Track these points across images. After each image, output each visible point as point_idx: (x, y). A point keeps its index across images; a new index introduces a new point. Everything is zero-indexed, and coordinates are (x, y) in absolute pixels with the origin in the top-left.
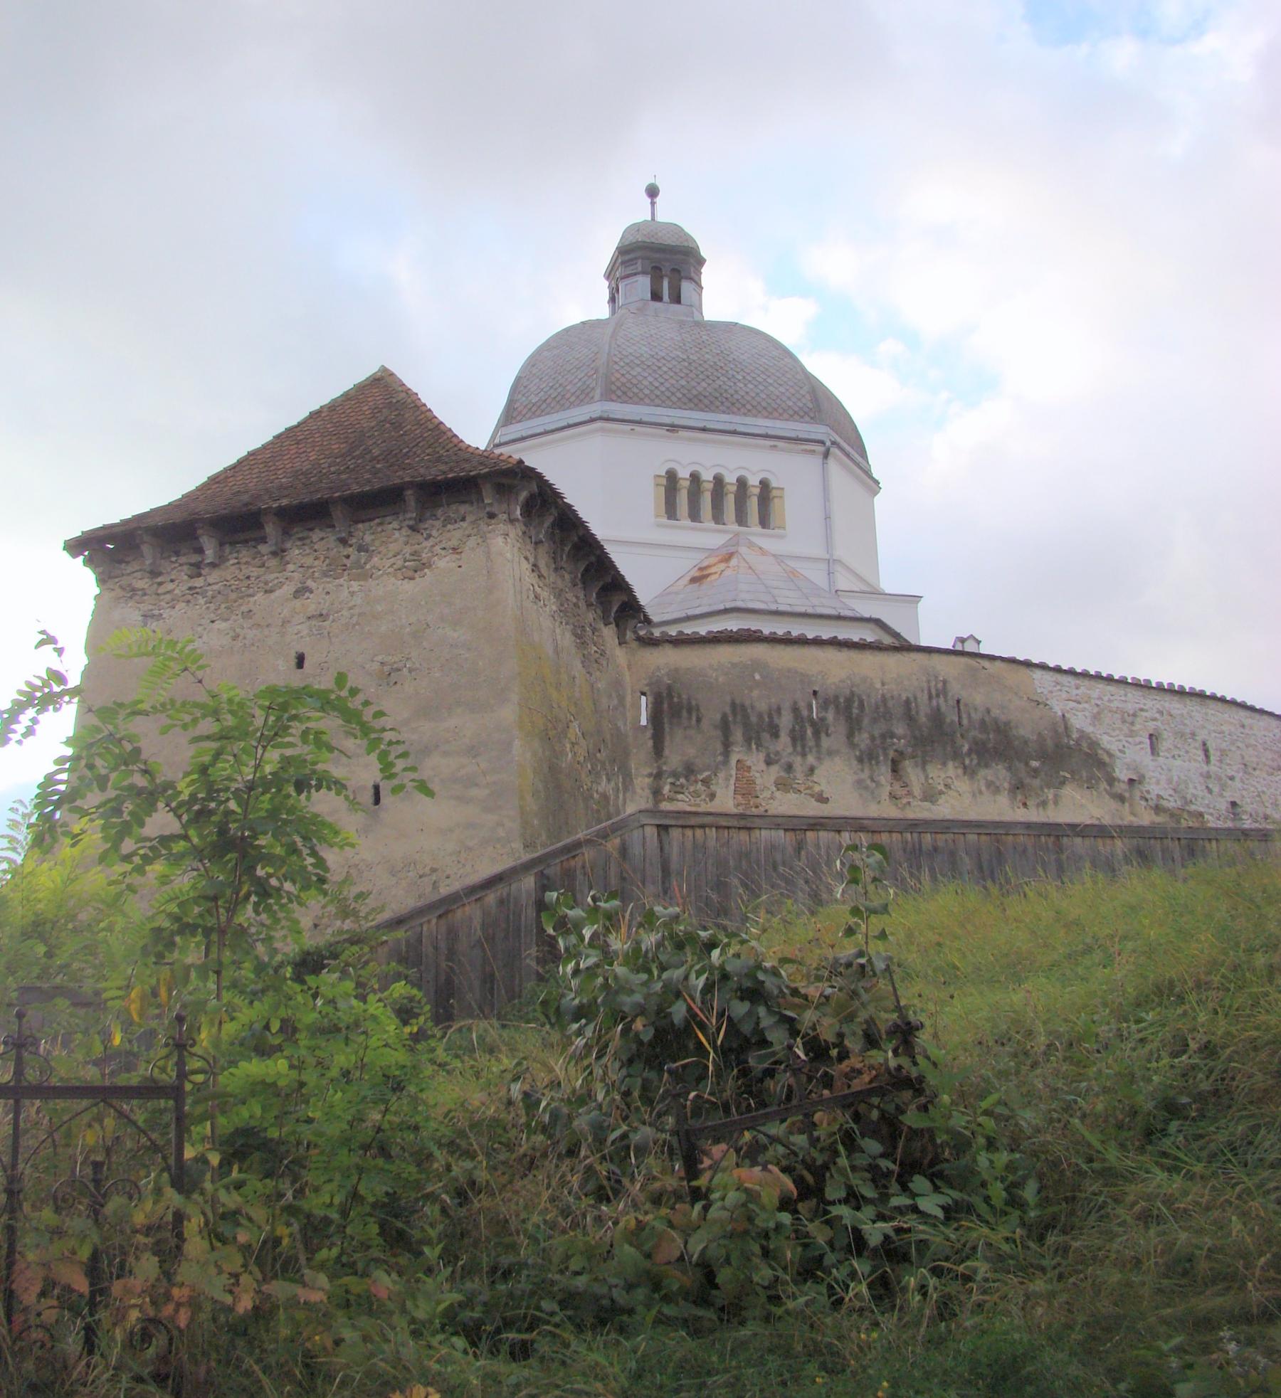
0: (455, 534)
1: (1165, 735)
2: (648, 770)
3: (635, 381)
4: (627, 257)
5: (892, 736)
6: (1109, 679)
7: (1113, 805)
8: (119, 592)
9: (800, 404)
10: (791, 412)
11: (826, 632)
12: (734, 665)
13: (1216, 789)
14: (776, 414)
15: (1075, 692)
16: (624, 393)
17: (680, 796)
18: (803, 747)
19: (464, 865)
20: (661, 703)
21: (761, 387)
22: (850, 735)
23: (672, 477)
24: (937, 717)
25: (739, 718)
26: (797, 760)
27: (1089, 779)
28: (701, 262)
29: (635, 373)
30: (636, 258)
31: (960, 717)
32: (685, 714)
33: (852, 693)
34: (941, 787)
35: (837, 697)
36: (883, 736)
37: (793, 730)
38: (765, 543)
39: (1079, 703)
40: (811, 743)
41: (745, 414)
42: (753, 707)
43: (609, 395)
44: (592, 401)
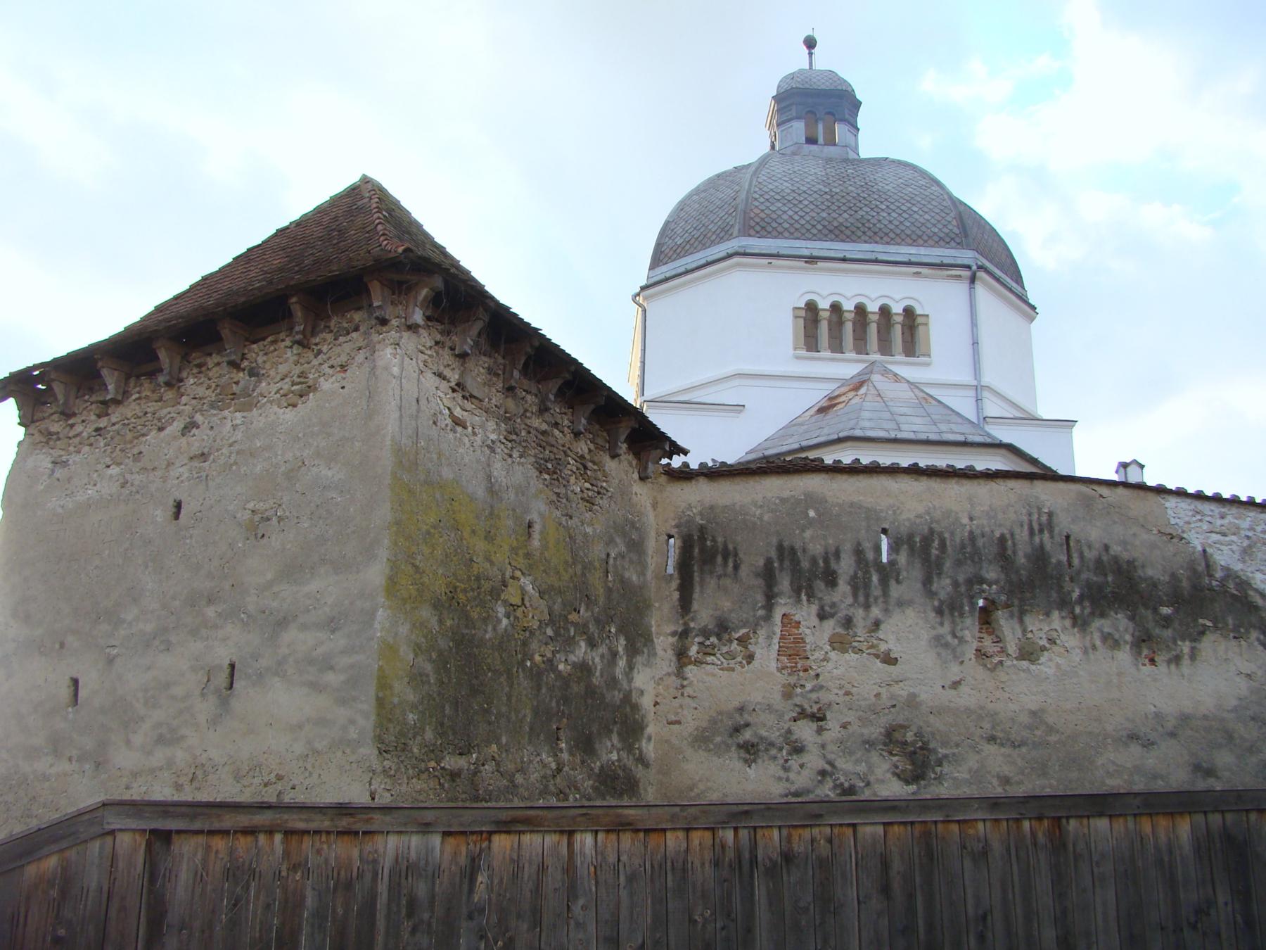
0: (344, 348)
2: (670, 628)
3: (774, 216)
4: (783, 105)
5: (982, 581)
8: (38, 437)
9: (946, 230)
10: (936, 239)
11: (905, 459)
12: (783, 500)
14: (921, 242)
15: (1219, 522)
17: (710, 659)
19: (311, 774)
20: (691, 547)
21: (906, 216)
22: (927, 582)
23: (811, 307)
24: (1040, 557)
25: (787, 563)
26: (859, 613)
28: (857, 105)
29: (774, 209)
30: (792, 104)
32: (719, 559)
33: (932, 531)
34: (1044, 642)
35: (911, 537)
36: (970, 582)
37: (854, 577)
38: (903, 371)
39: (1224, 535)
40: (876, 591)
41: (888, 243)
42: (804, 550)
43: (747, 231)
44: (730, 237)
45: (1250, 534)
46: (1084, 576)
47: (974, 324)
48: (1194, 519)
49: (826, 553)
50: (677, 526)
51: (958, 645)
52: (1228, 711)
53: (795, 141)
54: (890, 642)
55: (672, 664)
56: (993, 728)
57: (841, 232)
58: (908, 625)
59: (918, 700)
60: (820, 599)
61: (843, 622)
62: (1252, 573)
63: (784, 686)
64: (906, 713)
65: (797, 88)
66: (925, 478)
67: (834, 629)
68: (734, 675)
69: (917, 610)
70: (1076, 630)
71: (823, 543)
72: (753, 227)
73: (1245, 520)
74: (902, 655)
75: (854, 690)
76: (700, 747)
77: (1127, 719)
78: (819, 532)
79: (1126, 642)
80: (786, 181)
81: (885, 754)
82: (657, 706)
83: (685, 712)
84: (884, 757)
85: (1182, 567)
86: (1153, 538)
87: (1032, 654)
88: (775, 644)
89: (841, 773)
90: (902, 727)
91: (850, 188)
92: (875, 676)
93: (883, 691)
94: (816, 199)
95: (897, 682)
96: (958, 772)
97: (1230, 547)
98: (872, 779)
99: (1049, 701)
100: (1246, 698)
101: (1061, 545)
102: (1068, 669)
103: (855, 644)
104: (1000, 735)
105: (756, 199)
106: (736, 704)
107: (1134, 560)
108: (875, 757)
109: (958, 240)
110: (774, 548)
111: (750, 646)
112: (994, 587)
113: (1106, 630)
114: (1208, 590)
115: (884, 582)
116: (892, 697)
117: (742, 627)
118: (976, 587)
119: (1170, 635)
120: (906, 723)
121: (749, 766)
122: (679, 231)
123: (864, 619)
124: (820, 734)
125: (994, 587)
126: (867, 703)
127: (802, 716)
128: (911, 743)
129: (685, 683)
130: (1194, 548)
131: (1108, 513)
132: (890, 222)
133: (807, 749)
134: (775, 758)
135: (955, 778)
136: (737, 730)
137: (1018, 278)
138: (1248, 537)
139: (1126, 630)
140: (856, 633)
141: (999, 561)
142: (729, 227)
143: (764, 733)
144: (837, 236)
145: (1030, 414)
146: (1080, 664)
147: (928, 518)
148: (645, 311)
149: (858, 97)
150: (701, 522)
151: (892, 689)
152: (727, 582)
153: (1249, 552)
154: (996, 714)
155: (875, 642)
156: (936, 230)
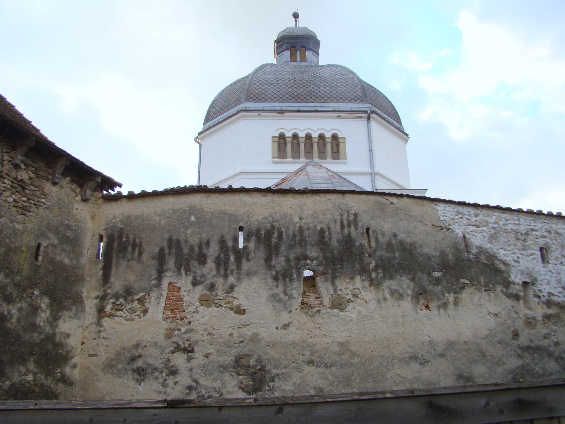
1: (554, 247)
3: (263, 92)
5: (306, 258)
6: (508, 210)
7: (509, 302)
9: (355, 95)
10: (350, 99)
12: (174, 211)
15: (474, 219)
17: (118, 313)
18: (226, 270)
21: (333, 88)
22: (268, 260)
23: (282, 137)
24: (348, 242)
25: (173, 250)
26: (220, 281)
27: (486, 285)
28: (317, 43)
31: (369, 242)
32: (130, 249)
33: (273, 227)
34: (350, 297)
35: (258, 231)
36: (298, 259)
39: (478, 227)
42: (186, 242)
43: (248, 100)
44: (241, 103)
45: (496, 226)
46: (378, 253)
48: (457, 217)
49: (201, 243)
50: (105, 230)
52: (482, 338)
53: (285, 61)
54: (241, 299)
55: (95, 317)
56: (312, 354)
57: (299, 98)
58: (253, 288)
59: (259, 337)
60: (195, 272)
61: (209, 287)
62: (498, 250)
63: (166, 330)
64: (250, 346)
65: (286, 35)
66: (271, 194)
68: (134, 323)
69: (260, 278)
70: (372, 288)
71: (199, 236)
72: (252, 98)
73: (492, 218)
75: (214, 332)
76: (108, 371)
77: (409, 346)
78: (197, 229)
79: (408, 295)
80: (272, 75)
81: (234, 374)
82: (83, 345)
83: (101, 348)
84: (233, 376)
85: (448, 247)
86: (428, 228)
87: (341, 305)
88: (162, 303)
89: (203, 387)
93: (235, 332)
94: (287, 83)
95: (245, 326)
96: (286, 385)
97: (482, 234)
98: (224, 391)
99: (353, 336)
100: (494, 329)
101: (363, 234)
102: (367, 314)
103: (217, 301)
104: (317, 359)
105: (254, 84)
106: (134, 342)
107: (415, 243)
108: (226, 376)
109: (361, 99)
110: (166, 241)
111: (146, 304)
112: (315, 261)
113: (394, 287)
114: (467, 261)
115: (238, 261)
116: (241, 335)
117: (141, 292)
118: (302, 262)
119: (440, 290)
120: (250, 353)
121: (140, 384)
122: (218, 104)
123: (223, 284)
124: (189, 362)
125: (315, 261)
126: (223, 340)
127: (177, 349)
129: (102, 329)
130: (457, 235)
131: (397, 214)
132: (325, 92)
134: (157, 378)
135: (284, 389)
136: (133, 359)
137: (398, 120)
138: (494, 228)
139: (408, 287)
140: (217, 293)
142: (240, 98)
143: (150, 361)
144: (296, 100)
145: (403, 187)
146: (375, 311)
148: (201, 146)
150: (120, 226)
151: (241, 330)
152: (134, 263)
153: (495, 237)
154: (313, 345)
155: (231, 299)
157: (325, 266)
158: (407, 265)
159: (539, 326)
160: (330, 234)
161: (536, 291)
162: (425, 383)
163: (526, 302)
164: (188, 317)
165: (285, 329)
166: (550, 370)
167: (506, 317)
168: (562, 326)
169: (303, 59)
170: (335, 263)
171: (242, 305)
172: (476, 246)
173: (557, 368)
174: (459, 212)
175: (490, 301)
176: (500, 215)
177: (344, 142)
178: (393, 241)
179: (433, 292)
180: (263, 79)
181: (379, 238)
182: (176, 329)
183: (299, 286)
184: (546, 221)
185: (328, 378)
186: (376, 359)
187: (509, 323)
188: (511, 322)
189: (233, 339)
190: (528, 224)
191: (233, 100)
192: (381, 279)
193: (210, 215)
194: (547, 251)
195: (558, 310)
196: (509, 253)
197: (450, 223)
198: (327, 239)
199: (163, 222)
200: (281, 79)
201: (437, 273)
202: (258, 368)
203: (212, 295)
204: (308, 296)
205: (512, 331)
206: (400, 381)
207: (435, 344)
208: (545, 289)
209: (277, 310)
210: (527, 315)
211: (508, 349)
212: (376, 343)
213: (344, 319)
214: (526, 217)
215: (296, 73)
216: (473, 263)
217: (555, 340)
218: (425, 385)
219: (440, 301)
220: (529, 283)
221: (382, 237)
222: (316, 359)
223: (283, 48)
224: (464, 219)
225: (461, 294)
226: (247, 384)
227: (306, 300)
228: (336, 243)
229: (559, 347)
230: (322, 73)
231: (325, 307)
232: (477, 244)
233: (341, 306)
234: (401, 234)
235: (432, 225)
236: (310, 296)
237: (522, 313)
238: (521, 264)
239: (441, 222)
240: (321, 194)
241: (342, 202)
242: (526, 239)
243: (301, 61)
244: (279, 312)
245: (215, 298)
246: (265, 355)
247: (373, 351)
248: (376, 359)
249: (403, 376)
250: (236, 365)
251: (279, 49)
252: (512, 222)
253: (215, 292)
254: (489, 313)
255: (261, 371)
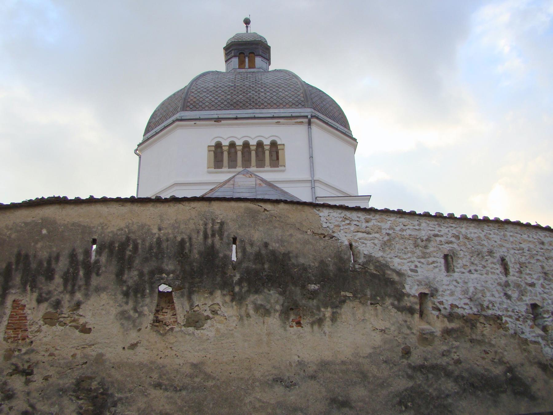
3: (201, 100)
5: (161, 271)
7: (400, 317)
9: (296, 99)
10: (291, 104)
12: (26, 224)
13: (515, 295)
14: (282, 106)
15: (364, 225)
16: (194, 106)
18: (73, 286)
21: (274, 94)
22: (120, 274)
23: (218, 146)
25: (21, 265)
27: (373, 297)
33: (128, 239)
34: (208, 313)
35: (112, 244)
36: (152, 273)
39: (368, 233)
40: (81, 282)
42: (35, 256)
43: (184, 108)
45: (390, 232)
47: (310, 147)
48: (343, 223)
49: (50, 257)
51: (138, 318)
52: (364, 357)
56: (160, 377)
57: (238, 105)
59: (104, 358)
60: (41, 289)
61: (54, 304)
62: (391, 258)
64: (94, 368)
65: (234, 42)
67: (47, 309)
69: (110, 294)
70: (234, 303)
74: (95, 326)
75: (56, 352)
77: (274, 367)
78: (48, 243)
79: (276, 311)
81: (74, 398)
84: (72, 400)
85: (330, 256)
86: (306, 237)
87: (197, 322)
90: (91, 378)
91: (246, 83)
92: (74, 341)
93: (78, 352)
94: (226, 90)
95: (90, 346)
96: (129, 411)
97: (372, 241)
99: (208, 356)
100: (380, 347)
102: (226, 332)
103: (62, 319)
104: (166, 382)
105: (193, 92)
107: (289, 252)
108: (66, 401)
109: (303, 104)
112: (171, 275)
113: (259, 302)
115: (88, 276)
116: (85, 356)
119: (315, 304)
123: (69, 301)
124: (27, 385)
125: (171, 275)
126: (65, 361)
127: (16, 371)
128: (95, 389)
133: (16, 396)
138: (388, 234)
139: (277, 302)
140: (62, 311)
141: (177, 258)
145: (348, 194)
146: (236, 328)
147: (127, 230)
148: (140, 158)
149: (269, 44)
151: (85, 351)
153: (388, 244)
154: (163, 367)
155: (77, 317)
156: (291, 100)
157: (182, 280)
158: (278, 277)
159: (437, 342)
160: (191, 245)
161: (436, 303)
162: (290, 408)
163: (422, 314)
164: (30, 337)
165: (133, 349)
166: (447, 392)
167: (396, 333)
168: (465, 341)
169: (252, 65)
170: (193, 277)
171: (88, 324)
172: (365, 254)
173: (455, 389)
174: (347, 218)
175: (377, 316)
176: (397, 219)
177: (283, 149)
178: (264, 251)
179: (306, 307)
180: (202, 87)
181: (247, 247)
182: (16, 350)
183: (151, 302)
184: (453, 225)
185: (176, 403)
186: (233, 382)
187: (399, 341)
188: (402, 338)
189: (76, 360)
190: (431, 229)
191: (171, 110)
192: (245, 293)
193: (62, 227)
194: (452, 258)
195: (462, 324)
196: (405, 261)
197: (334, 230)
198: (187, 251)
199: (13, 236)
200: (220, 87)
201: (313, 285)
202: (100, 392)
203: (57, 312)
204: (165, 313)
205: (402, 349)
206: (261, 406)
207: (305, 365)
208: (447, 300)
209: (125, 328)
210: (423, 330)
211: (395, 369)
212: (235, 364)
213: (199, 337)
214: (429, 221)
215: (237, 79)
216: (359, 273)
217: (456, 357)
218: (290, 411)
219: (314, 317)
220: (428, 294)
221: (250, 248)
222: (165, 382)
223: (231, 55)
224: (353, 225)
225: (341, 308)
226: (86, 409)
227: (161, 317)
228: (197, 255)
229: (460, 366)
230: (265, 79)
231: (179, 324)
232: (366, 252)
233: (197, 324)
234: (274, 244)
235: (312, 233)
236: (167, 313)
237: (416, 328)
238: (419, 273)
239: (324, 229)
240: (185, 202)
241: (207, 210)
242: (427, 246)
243: (249, 68)
244: (126, 331)
245: (60, 316)
246: (109, 377)
247: (231, 373)
248: (233, 382)
249: (265, 400)
250: (77, 388)
251: (228, 56)
252: (412, 227)
253: (60, 309)
254: (374, 329)
255: (103, 395)
